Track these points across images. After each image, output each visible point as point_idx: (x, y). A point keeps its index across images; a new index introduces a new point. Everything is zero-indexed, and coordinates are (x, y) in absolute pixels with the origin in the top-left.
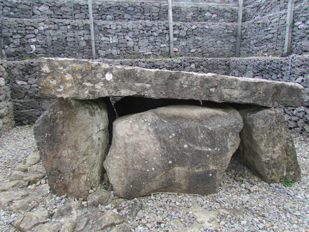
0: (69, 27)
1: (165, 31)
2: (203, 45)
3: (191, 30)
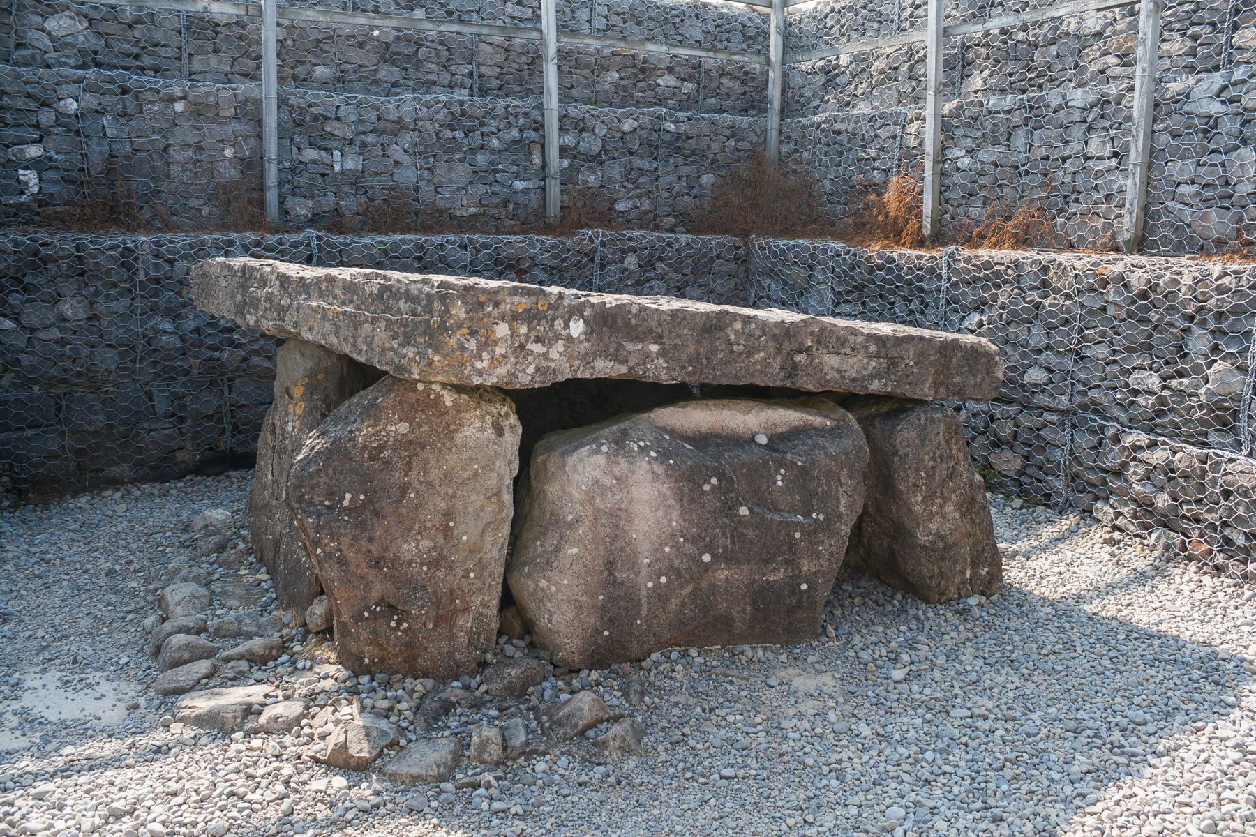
0: (179, 107)
1: (531, 134)
2: (657, 188)
3: (620, 134)
